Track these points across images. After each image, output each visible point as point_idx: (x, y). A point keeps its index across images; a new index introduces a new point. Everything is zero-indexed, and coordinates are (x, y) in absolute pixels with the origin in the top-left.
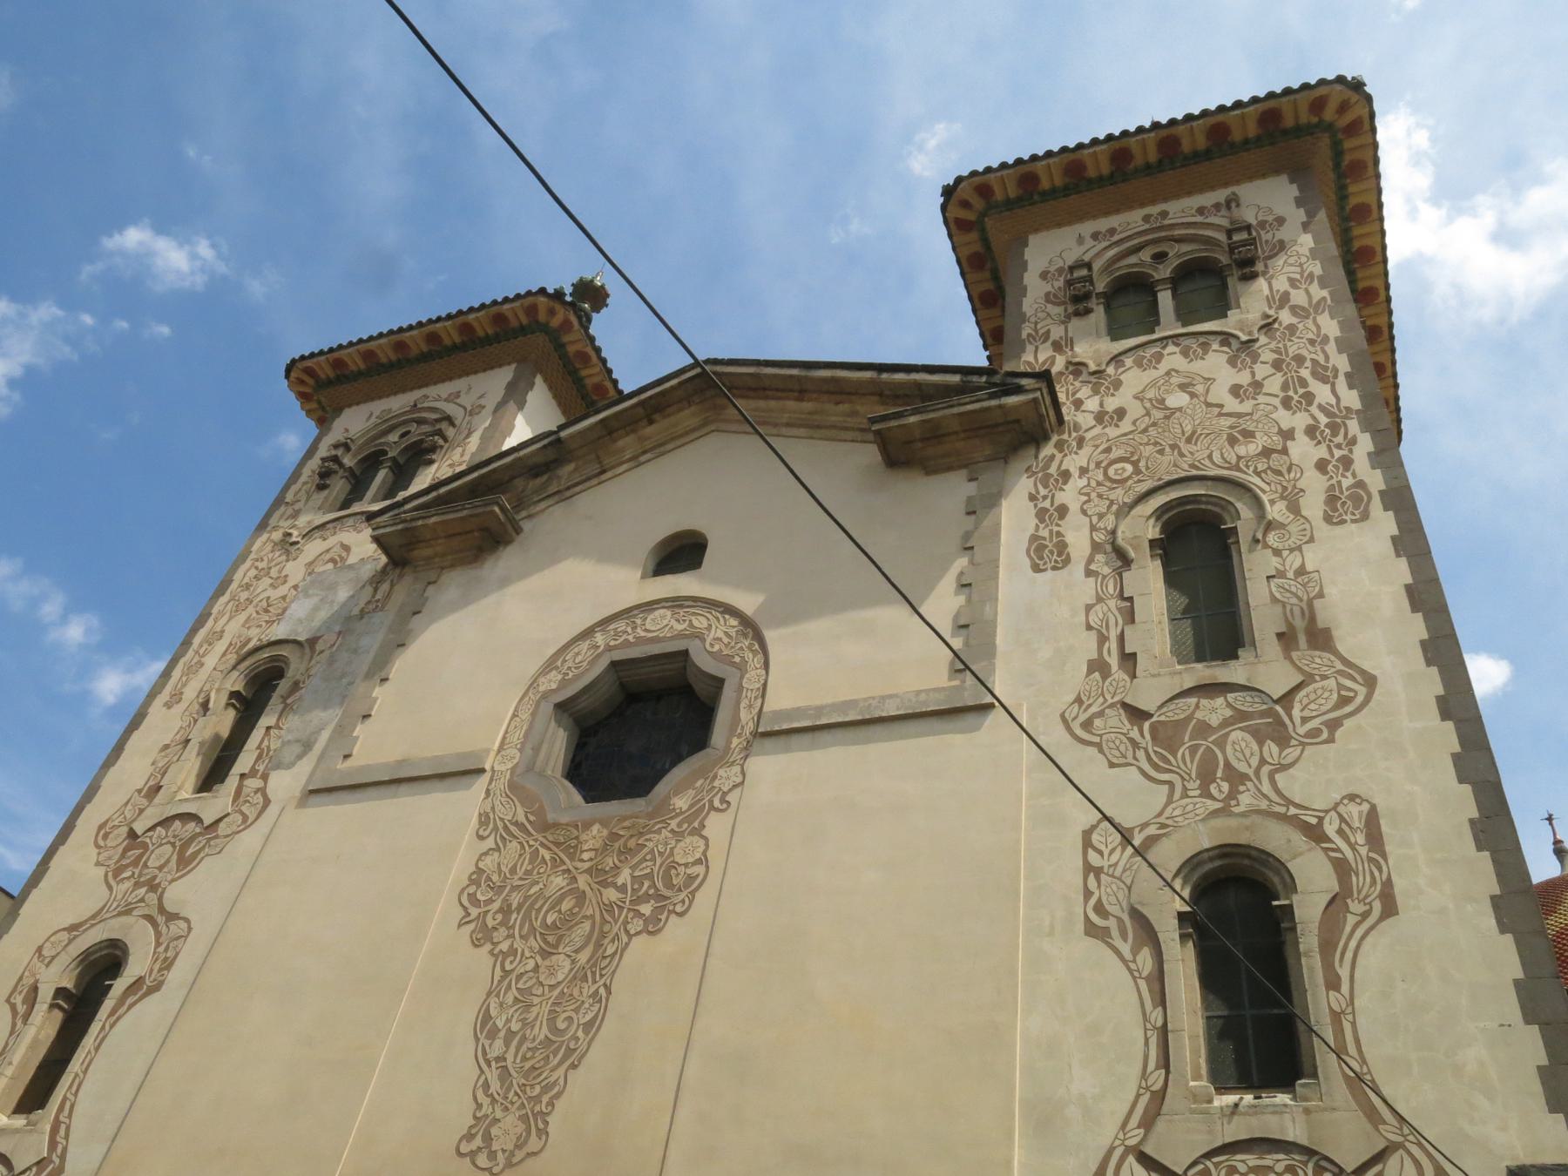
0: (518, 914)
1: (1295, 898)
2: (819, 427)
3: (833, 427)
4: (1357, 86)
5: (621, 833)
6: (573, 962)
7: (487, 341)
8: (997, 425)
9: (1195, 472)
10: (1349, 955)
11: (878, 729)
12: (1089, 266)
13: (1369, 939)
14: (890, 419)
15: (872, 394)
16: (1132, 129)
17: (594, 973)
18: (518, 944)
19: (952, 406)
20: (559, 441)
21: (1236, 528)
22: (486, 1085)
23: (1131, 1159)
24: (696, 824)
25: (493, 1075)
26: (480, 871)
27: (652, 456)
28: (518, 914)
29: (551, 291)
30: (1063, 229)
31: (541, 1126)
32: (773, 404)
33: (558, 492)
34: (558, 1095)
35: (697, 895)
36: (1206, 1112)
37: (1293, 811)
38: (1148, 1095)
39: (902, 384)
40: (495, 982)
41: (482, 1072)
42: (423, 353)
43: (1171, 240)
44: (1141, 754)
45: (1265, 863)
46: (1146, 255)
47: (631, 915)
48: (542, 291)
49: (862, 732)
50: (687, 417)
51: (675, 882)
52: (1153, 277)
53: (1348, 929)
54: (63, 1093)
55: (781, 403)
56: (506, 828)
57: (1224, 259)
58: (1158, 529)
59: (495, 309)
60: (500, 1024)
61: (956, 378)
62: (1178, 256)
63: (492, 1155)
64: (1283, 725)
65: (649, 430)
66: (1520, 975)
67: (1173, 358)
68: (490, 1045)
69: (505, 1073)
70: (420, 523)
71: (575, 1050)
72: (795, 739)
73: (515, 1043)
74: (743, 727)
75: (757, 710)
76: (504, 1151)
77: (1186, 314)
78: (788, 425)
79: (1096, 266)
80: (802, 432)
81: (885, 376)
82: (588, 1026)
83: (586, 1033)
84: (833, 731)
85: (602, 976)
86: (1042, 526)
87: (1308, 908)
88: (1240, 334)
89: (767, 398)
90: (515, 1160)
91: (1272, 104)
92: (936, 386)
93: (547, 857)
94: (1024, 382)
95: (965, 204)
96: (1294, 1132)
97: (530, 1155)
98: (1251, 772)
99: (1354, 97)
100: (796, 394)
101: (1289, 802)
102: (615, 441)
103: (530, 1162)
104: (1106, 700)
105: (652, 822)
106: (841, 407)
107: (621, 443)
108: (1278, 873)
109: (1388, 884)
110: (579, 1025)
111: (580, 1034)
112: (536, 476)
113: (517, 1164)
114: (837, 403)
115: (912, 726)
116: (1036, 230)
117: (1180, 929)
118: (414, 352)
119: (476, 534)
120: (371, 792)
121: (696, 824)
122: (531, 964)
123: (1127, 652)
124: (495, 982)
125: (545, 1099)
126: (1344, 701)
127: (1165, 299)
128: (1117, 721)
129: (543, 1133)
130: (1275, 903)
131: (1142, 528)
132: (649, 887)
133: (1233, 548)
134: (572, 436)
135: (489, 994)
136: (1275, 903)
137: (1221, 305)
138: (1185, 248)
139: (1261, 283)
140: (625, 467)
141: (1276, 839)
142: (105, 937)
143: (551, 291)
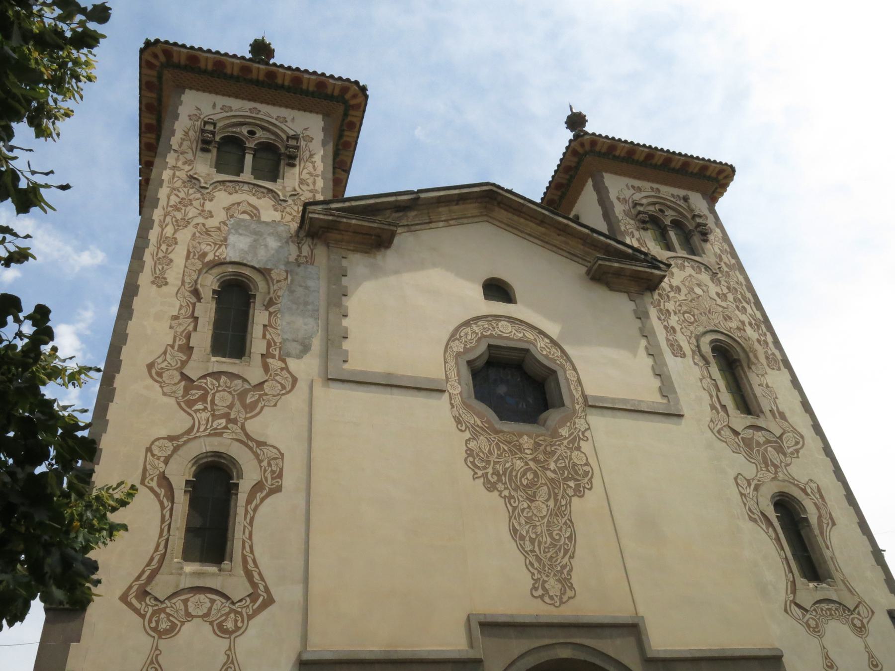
0: (505, 477)
1: (241, 480)
2: (547, 243)
3: (555, 246)
4: (364, 89)
5: (541, 442)
6: (547, 506)
7: (307, 93)
8: (642, 279)
9: (716, 329)
10: (828, 538)
11: (640, 415)
12: (215, 125)
13: (832, 533)
14: (607, 261)
15: (581, 239)
16: (604, 135)
17: (560, 513)
18: (513, 493)
19: (631, 265)
20: (418, 198)
21: (255, 295)
22: (531, 564)
23: (793, 605)
24: (576, 445)
25: (533, 560)
26: (469, 449)
27: (456, 223)
28: (505, 477)
29: (361, 84)
30: (224, 97)
31: (569, 585)
32: (522, 220)
33: (407, 225)
34: (571, 570)
35: (593, 480)
36: (808, 589)
37: (796, 482)
38: (790, 583)
39: (599, 241)
40: (511, 512)
41: (526, 557)
42: (332, 95)
43: (258, 126)
44: (741, 449)
45: (234, 464)
46: (245, 130)
47: (565, 486)
48: (356, 83)
49: (635, 415)
50: (472, 208)
51: (580, 473)
52: (246, 144)
53: (825, 528)
54: (240, 554)
55: (527, 222)
56: (473, 427)
57: (283, 150)
58: (217, 284)
59: (297, 73)
60: (524, 534)
61: (630, 251)
62: (260, 138)
63: (551, 598)
64: (782, 447)
65: (456, 208)
66: (872, 550)
67: (244, 197)
68: (524, 544)
69: (539, 559)
70: (345, 220)
71: (569, 549)
72: (605, 412)
73: (536, 544)
74: (577, 400)
75: (580, 391)
76: (557, 596)
77: (257, 172)
78: (530, 235)
79: (219, 125)
80: (539, 242)
81: (595, 235)
82: (570, 538)
83: (571, 541)
84: (650, 415)
85: (565, 515)
86: (669, 334)
87: (245, 486)
88: (202, 181)
89: (519, 216)
90: (564, 600)
91: (708, 163)
92: (616, 249)
93: (506, 448)
94: (661, 265)
95: (582, 145)
96: (835, 598)
97: (570, 598)
98: (779, 464)
99: (360, 94)
100: (538, 222)
101: (794, 479)
102: (438, 207)
103: (571, 601)
104: (722, 424)
105: (554, 440)
106: (560, 238)
107: (441, 209)
108: (797, 504)
109: (830, 514)
110: (565, 538)
111: (567, 542)
112: (397, 211)
113: (566, 602)
114: (559, 235)
115: (652, 417)
116: (191, 88)
117: (185, 487)
118: (254, 76)
119: (373, 237)
120: (373, 388)
121: (576, 445)
122: (525, 505)
123: (190, 345)
124: (511, 512)
125: (565, 571)
126: (797, 443)
127: (249, 159)
128: (727, 433)
129: (572, 588)
130: (231, 481)
131: (210, 283)
132: (568, 474)
133: (252, 305)
134: (425, 199)
135: (510, 518)
136: (231, 481)
137: (274, 176)
138: (268, 135)
139: (296, 170)
140: (441, 224)
141: (238, 452)
142: (209, 449)
143: (361, 84)
